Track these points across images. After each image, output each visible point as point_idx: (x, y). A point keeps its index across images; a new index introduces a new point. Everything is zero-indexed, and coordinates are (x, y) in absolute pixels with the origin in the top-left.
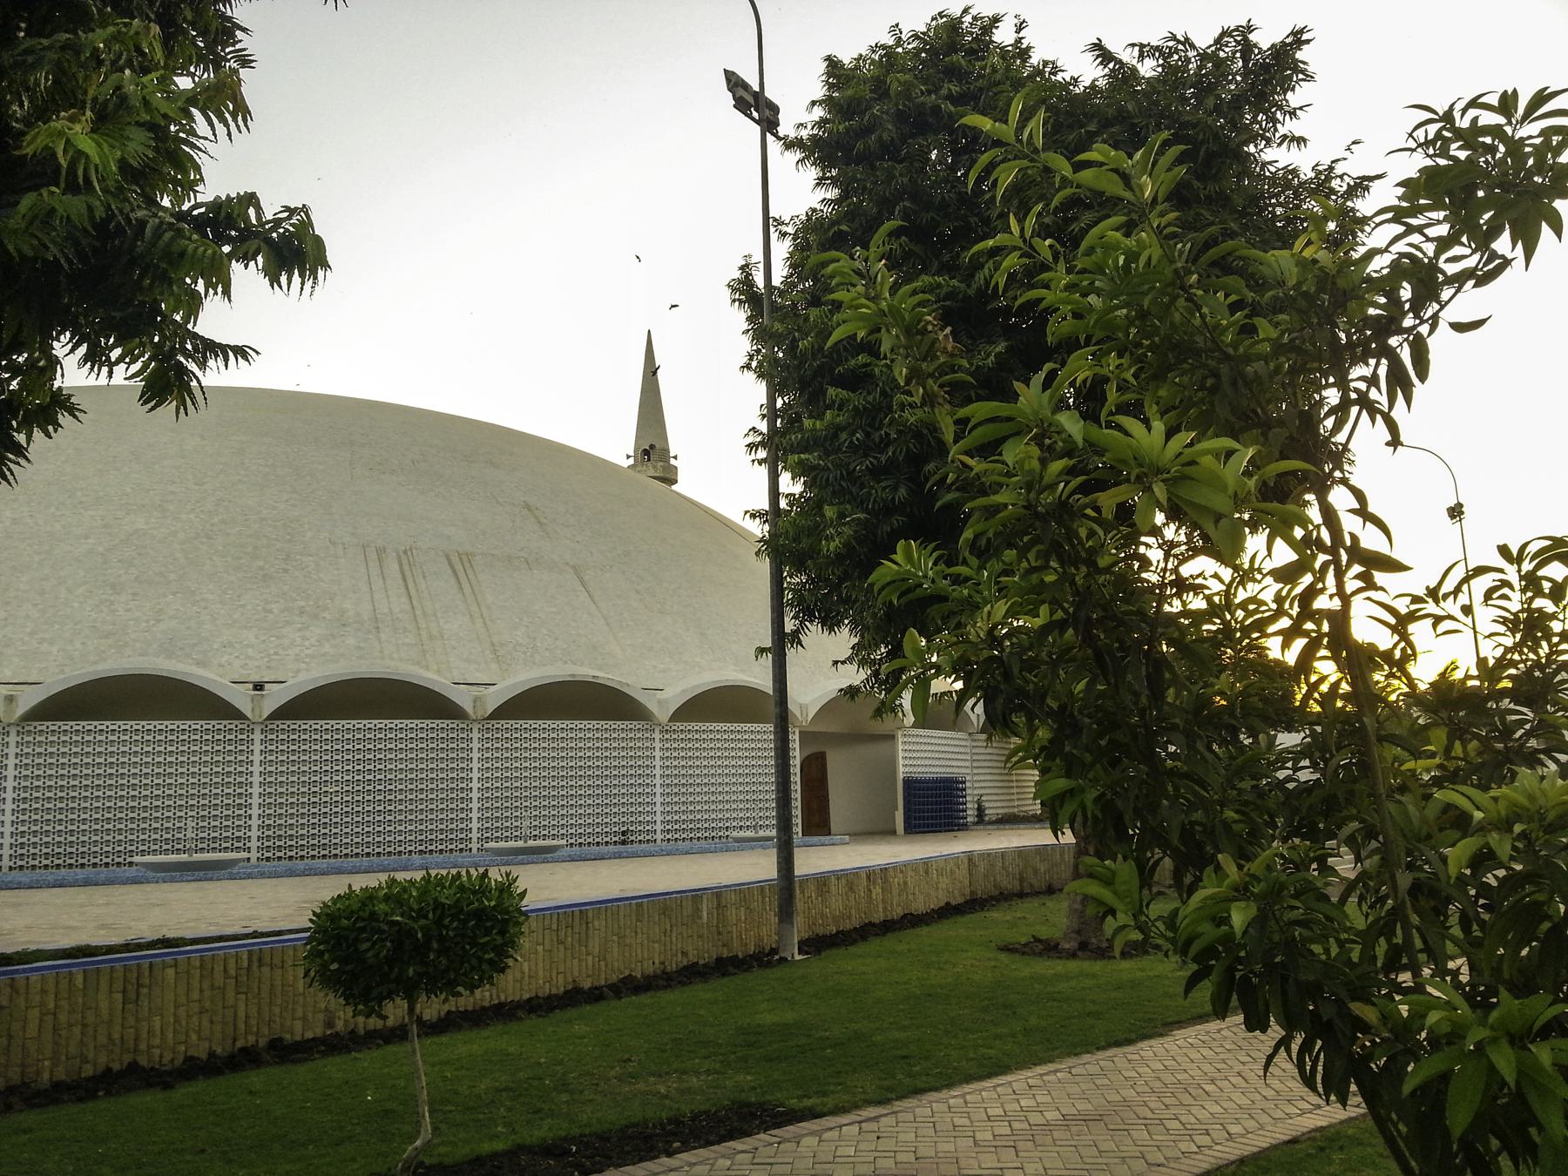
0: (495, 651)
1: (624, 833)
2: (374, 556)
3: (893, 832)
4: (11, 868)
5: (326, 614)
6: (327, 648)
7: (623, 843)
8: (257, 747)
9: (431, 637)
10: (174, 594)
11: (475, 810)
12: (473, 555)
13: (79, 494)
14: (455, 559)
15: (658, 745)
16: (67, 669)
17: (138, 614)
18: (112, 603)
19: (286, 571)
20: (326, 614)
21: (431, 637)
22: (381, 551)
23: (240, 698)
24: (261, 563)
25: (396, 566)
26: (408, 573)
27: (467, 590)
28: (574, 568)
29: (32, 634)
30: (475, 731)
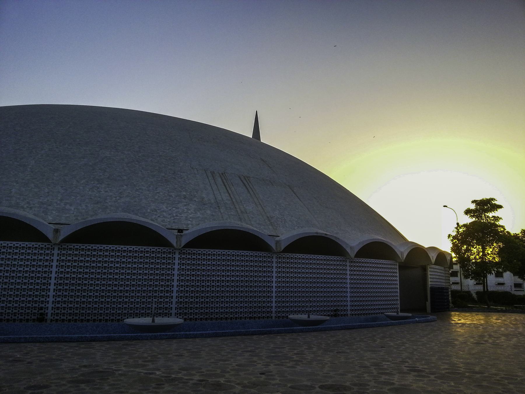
0: (269, 220)
1: (335, 311)
2: (210, 174)
3: (423, 310)
4: (51, 320)
5: (195, 199)
6: (199, 214)
7: (335, 316)
8: (177, 262)
9: (242, 212)
10: (127, 185)
11: (176, 275)
12: (249, 177)
13: (78, 140)
14: (242, 178)
15: (348, 268)
16: (79, 218)
17: (111, 194)
18: (98, 188)
19: (175, 178)
20: (195, 199)
21: (242, 212)
22: (213, 173)
23: (172, 239)
24: (163, 174)
25: (220, 179)
26: (226, 184)
27: (251, 192)
28: (289, 186)
29: (61, 200)
30: (274, 257)
